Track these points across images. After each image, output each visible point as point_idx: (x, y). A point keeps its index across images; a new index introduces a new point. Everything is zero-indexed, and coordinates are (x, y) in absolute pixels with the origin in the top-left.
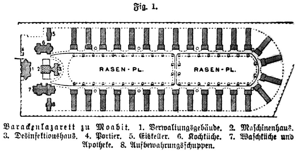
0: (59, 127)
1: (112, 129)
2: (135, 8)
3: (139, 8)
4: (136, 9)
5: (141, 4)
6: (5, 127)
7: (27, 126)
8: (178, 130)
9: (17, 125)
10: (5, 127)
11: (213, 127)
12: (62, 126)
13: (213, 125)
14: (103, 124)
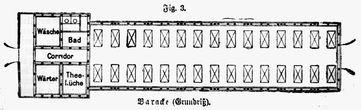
0: (150, 102)
1: (146, 104)
2: (164, 9)
3: (168, 9)
4: (166, 10)
5: (170, 5)
6: (140, 102)
7: (161, 101)
8: (185, 104)
9: (152, 100)
10: (140, 102)
11: (193, 101)
12: (154, 101)
13: (193, 99)
14: (143, 99)
